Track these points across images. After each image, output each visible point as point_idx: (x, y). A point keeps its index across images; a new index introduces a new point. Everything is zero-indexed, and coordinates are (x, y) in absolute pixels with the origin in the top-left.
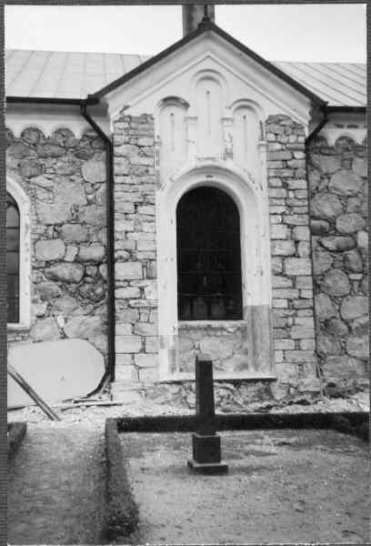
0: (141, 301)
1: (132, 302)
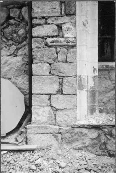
1: (49, 40)
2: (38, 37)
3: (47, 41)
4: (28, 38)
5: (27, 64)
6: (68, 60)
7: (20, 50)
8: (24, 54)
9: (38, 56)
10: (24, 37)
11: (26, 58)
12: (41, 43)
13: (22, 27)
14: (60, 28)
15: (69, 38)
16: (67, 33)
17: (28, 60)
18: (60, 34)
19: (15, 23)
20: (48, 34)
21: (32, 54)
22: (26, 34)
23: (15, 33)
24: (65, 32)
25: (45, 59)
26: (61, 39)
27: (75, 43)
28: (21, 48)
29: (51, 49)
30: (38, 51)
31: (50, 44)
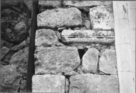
0: (84, 31)
1: (67, 33)
2: (46, 28)
3: (62, 34)
4: (30, 35)
5: (25, 77)
6: (101, 69)
7: (16, 54)
8: (22, 61)
9: (45, 61)
10: (23, 34)
11: (23, 68)
12: (52, 37)
13: (21, 19)
14: (85, 15)
15: (102, 30)
16: (99, 22)
17: (26, 72)
18: (85, 24)
19: (11, 12)
20: (66, 23)
21: (34, 56)
22: (28, 29)
23: (9, 28)
24: (95, 20)
25: (58, 67)
26: (87, 31)
27: (113, 39)
28: (17, 51)
29: (69, 48)
30: (46, 52)
31: (68, 40)
